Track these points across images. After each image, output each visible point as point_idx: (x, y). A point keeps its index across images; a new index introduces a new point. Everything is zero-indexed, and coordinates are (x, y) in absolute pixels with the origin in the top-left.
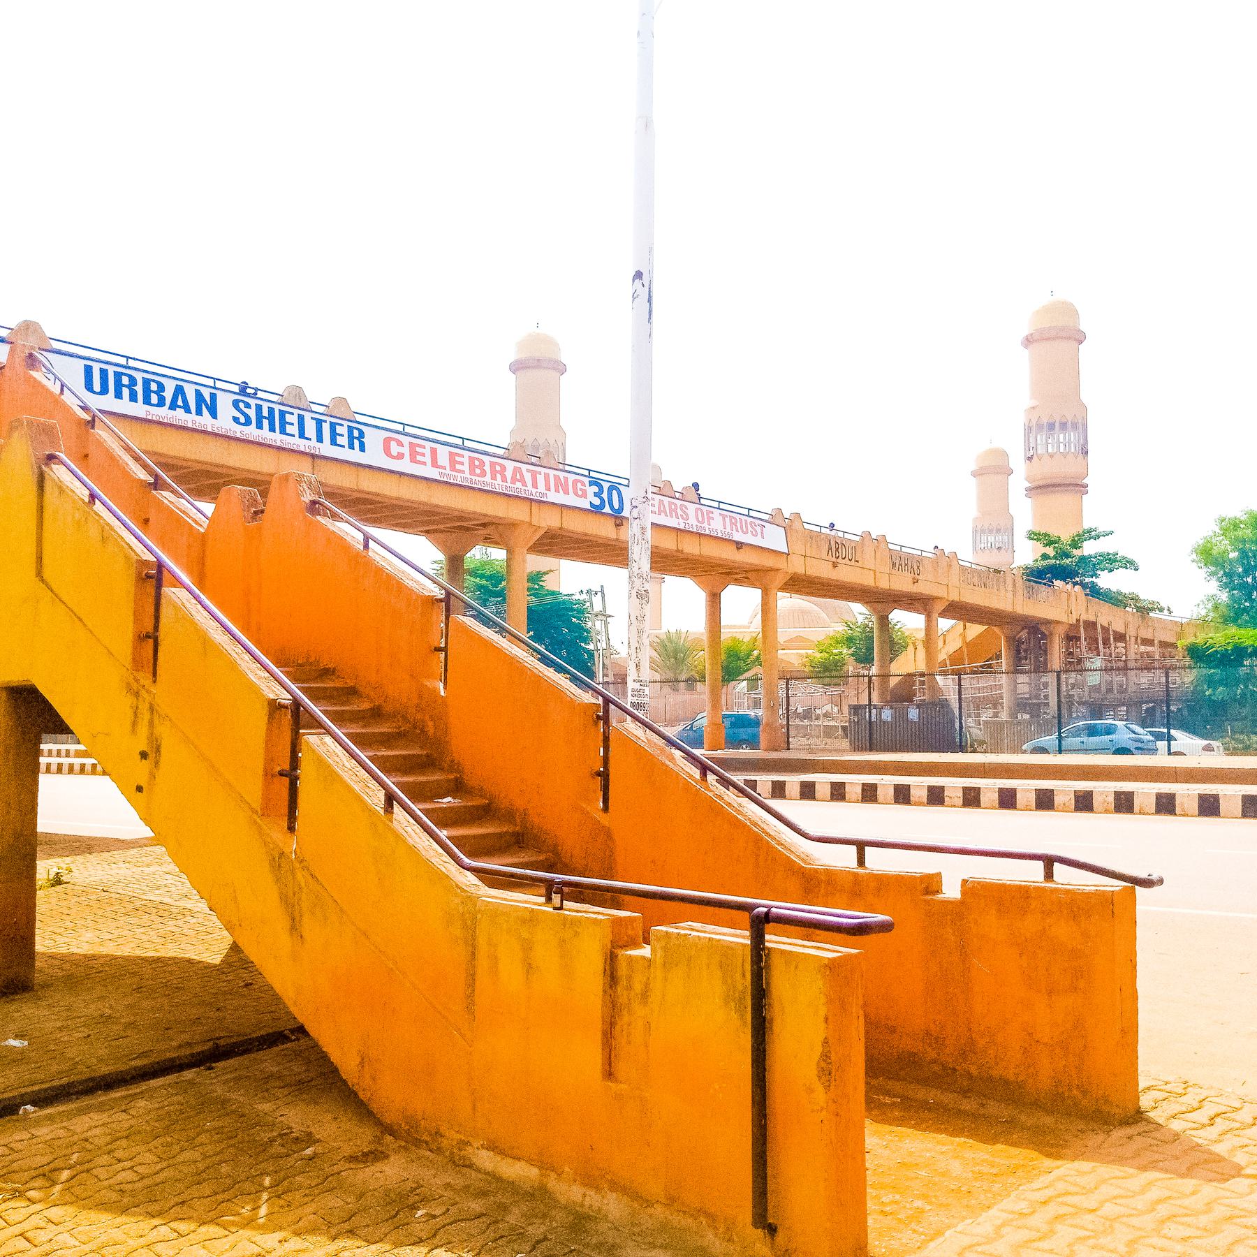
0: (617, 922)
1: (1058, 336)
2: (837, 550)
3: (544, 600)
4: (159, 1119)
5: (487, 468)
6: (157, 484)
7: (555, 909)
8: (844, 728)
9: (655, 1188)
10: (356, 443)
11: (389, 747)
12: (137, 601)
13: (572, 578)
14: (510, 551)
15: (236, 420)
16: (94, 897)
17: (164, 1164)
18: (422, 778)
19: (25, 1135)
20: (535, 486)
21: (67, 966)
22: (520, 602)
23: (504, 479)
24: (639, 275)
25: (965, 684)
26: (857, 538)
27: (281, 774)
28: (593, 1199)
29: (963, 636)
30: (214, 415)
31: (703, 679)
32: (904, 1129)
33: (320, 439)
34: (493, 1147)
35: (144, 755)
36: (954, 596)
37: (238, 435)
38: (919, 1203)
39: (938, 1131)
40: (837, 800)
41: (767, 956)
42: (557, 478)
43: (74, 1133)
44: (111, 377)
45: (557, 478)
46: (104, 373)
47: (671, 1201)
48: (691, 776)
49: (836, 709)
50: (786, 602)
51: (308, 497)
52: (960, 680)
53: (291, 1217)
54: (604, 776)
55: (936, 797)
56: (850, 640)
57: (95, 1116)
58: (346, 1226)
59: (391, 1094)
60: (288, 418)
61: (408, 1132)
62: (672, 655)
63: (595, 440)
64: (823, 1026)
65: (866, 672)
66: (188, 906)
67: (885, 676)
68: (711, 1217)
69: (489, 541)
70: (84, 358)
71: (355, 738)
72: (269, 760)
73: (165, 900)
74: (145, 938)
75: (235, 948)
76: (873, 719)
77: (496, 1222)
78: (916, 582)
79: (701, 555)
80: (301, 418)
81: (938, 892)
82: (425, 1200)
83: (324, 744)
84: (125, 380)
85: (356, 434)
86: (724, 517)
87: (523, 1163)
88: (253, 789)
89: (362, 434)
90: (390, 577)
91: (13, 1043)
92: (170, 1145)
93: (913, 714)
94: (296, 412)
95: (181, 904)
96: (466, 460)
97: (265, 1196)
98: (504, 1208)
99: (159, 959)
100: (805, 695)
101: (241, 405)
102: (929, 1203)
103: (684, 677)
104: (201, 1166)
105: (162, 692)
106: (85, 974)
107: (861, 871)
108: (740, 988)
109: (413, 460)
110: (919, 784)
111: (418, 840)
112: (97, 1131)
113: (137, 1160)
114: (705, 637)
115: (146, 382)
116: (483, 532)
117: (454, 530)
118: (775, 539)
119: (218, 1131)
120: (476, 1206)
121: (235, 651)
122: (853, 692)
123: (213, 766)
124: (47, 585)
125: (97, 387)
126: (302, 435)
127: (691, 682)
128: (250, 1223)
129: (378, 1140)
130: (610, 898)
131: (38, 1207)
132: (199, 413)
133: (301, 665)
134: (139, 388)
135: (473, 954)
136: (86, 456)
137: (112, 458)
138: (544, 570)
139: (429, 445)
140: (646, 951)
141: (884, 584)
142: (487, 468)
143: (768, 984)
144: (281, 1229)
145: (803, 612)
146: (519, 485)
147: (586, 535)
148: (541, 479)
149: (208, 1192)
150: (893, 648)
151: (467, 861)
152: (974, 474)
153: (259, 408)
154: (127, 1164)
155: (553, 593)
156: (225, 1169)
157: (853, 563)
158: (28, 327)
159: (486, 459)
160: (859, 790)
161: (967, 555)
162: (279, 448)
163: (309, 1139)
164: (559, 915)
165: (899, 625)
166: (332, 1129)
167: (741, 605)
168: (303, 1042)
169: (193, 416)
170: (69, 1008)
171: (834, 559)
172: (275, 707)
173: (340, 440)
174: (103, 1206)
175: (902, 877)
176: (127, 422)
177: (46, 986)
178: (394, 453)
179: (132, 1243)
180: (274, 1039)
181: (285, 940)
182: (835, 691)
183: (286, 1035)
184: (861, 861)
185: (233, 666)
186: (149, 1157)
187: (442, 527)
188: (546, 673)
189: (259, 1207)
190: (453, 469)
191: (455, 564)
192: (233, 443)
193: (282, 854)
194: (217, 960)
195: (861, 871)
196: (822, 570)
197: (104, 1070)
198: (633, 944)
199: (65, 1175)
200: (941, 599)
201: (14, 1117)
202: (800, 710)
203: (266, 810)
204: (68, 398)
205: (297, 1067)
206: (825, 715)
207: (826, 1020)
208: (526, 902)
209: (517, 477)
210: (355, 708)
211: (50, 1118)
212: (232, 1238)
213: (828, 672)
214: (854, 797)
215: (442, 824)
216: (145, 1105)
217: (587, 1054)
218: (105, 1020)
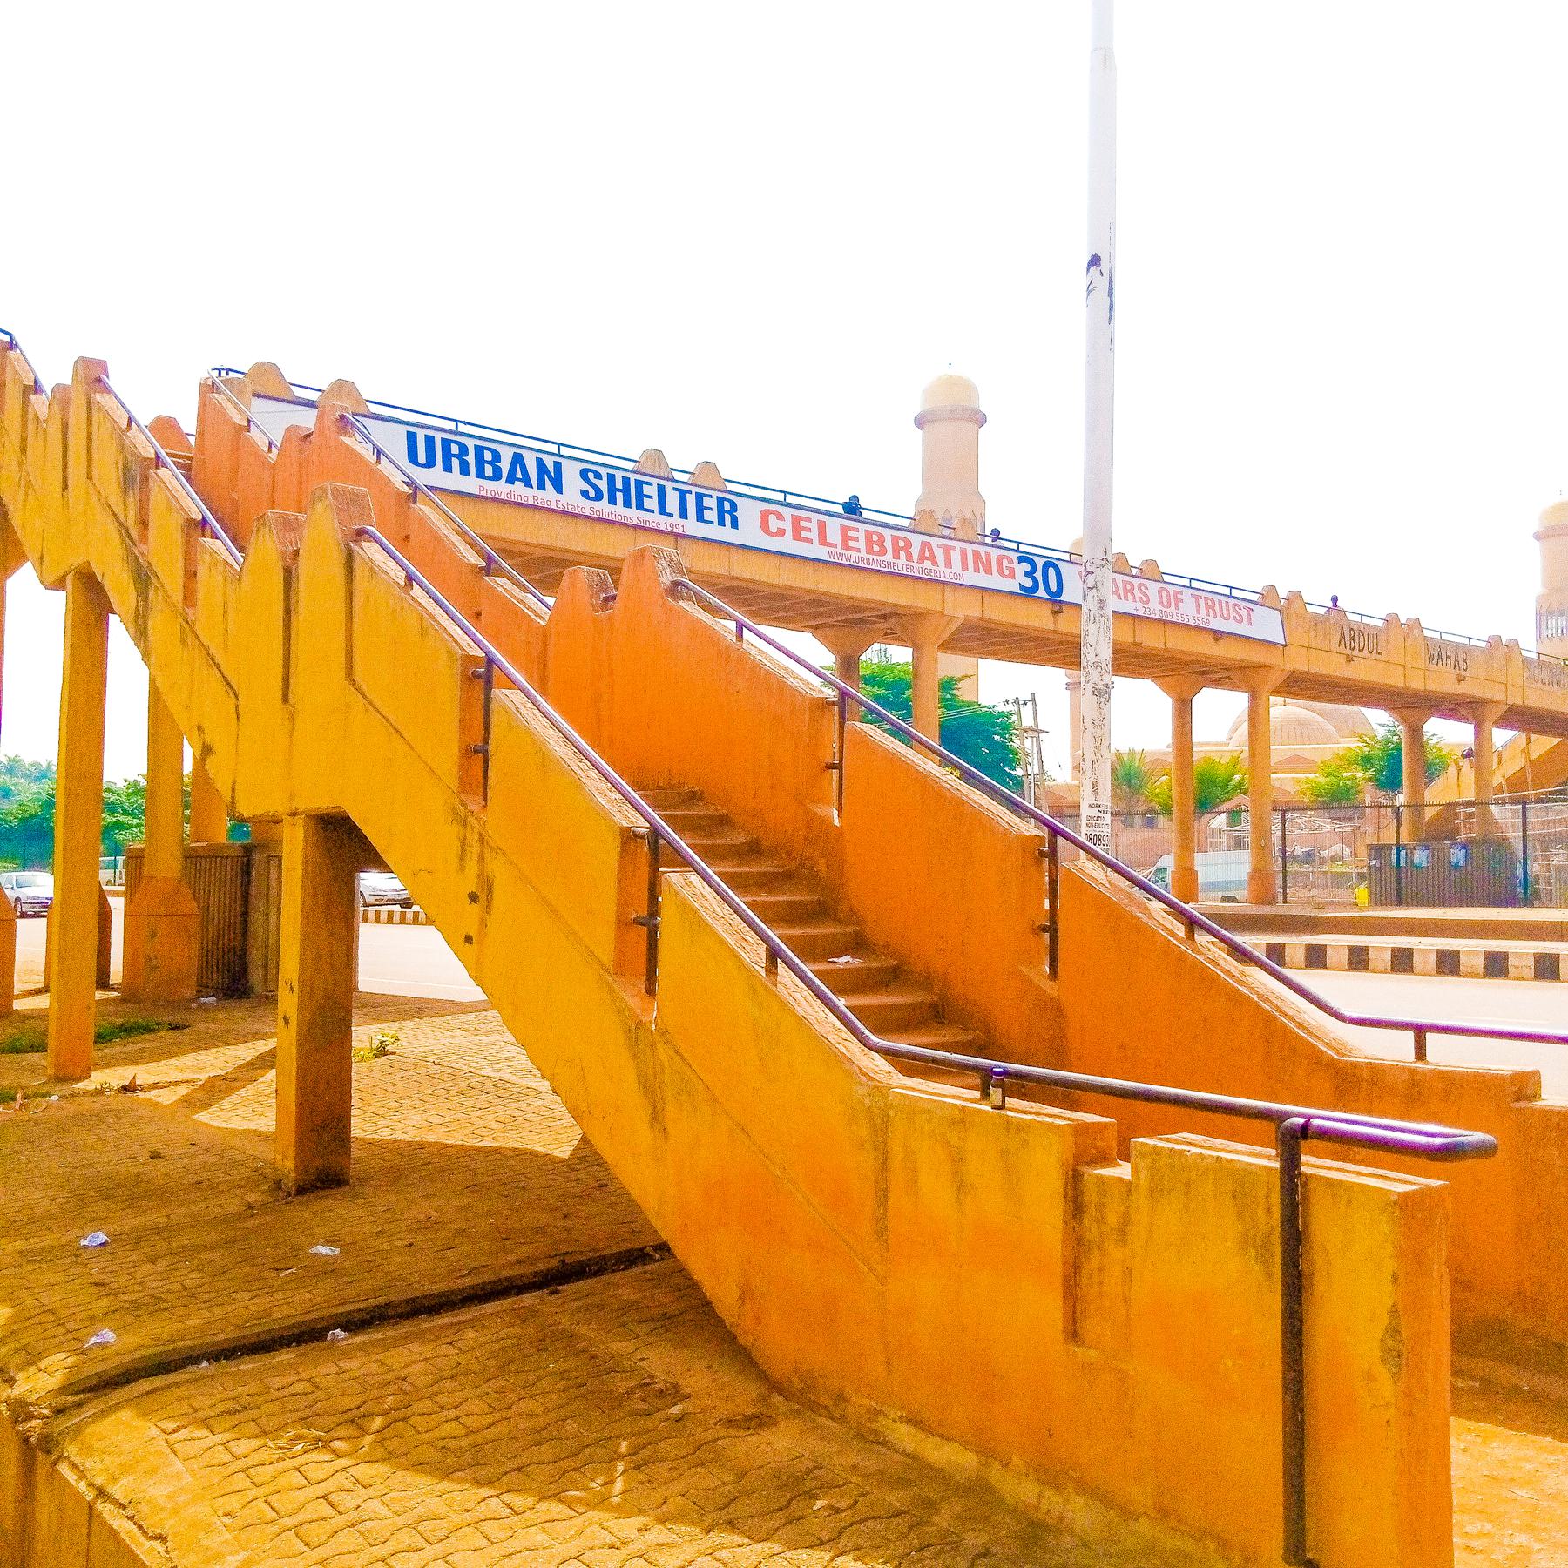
0: (1081, 1130)
2: (1352, 639)
3: (958, 713)
4: (491, 1355)
5: (888, 544)
6: (490, 568)
7: (995, 1108)
8: (1361, 877)
9: (1140, 1495)
10: (728, 518)
11: (770, 892)
12: (465, 706)
13: (996, 683)
14: (917, 649)
15: (585, 494)
16: (423, 1071)
17: (497, 1416)
18: (810, 931)
19: (333, 1369)
20: (948, 564)
21: (388, 1156)
22: (930, 717)
23: (909, 557)
24: (1095, 261)
25: (1531, 817)
26: (1380, 623)
27: (638, 922)
28: (1052, 1503)
29: (1526, 751)
30: (559, 490)
31: (1167, 812)
32: (1489, 1426)
33: (684, 515)
34: (914, 1421)
35: (473, 898)
36: (1515, 699)
37: (587, 513)
38: (1522, 1539)
39: (1537, 1432)
40: (1357, 969)
41: (1305, 1185)
42: (976, 554)
43: (390, 1369)
44: (440, 446)
45: (976, 554)
46: (430, 441)
47: (1163, 1513)
48: (1172, 934)
49: (1347, 851)
50: (1281, 709)
51: (667, 578)
52: (1524, 809)
53: (657, 1497)
54: (1052, 929)
55: (1496, 966)
56: (1366, 761)
57: (415, 1347)
58: (721, 1515)
59: (781, 1343)
60: (647, 490)
61: (801, 1391)
62: (1128, 779)
63: (1031, 503)
64: (1390, 1288)
65: (1389, 803)
66: (533, 1085)
67: (1417, 807)
68: (1223, 1544)
69: (890, 636)
70: (407, 424)
71: (729, 879)
72: (623, 903)
73: (508, 1077)
74: (481, 1123)
75: (584, 1140)
76: (1402, 864)
77: (920, 1524)
79: (1166, 649)
80: (661, 489)
81: (1536, 1096)
82: (827, 1486)
83: (689, 884)
84: (455, 449)
85: (727, 506)
86: (1197, 598)
87: (956, 1445)
88: (604, 942)
89: (734, 506)
90: (768, 675)
91: (322, 1250)
92: (502, 1391)
93: (1457, 856)
94: (655, 481)
95: (525, 1081)
96: (861, 536)
97: (621, 1467)
98: (930, 1505)
99: (496, 1151)
100: (1308, 831)
101: (591, 475)
102: (1541, 1541)
103: (1141, 808)
104: (543, 1421)
105: (495, 820)
106: (413, 1166)
107: (1420, 1065)
108: (1262, 1227)
109: (797, 537)
110: (1473, 949)
111: (810, 1010)
112: (416, 1368)
113: (464, 1408)
114: (1171, 759)
115: (479, 451)
116: (884, 626)
117: (848, 624)
118: (1267, 626)
119: (563, 1374)
120: (895, 1499)
121: (580, 767)
122: (1371, 829)
123: (555, 912)
124: (359, 690)
125: (422, 458)
126: (662, 510)
127: (1149, 818)
128: (602, 1502)
129: (763, 1399)
130: (1065, 1094)
131: (345, 1462)
132: (541, 486)
133: (660, 788)
134: (471, 458)
135: (885, 1162)
136: (408, 537)
137: (437, 539)
138: (957, 675)
139: (815, 517)
140: (1124, 1171)
141: (1417, 684)
142: (888, 544)
143: (1305, 1225)
144: (640, 1512)
145: (1301, 724)
146: (928, 564)
147: (1015, 626)
148: (956, 556)
149: (546, 1457)
150: (1428, 771)
151: (873, 1038)
152: (1537, 537)
153: (611, 478)
154: (453, 1413)
155: (970, 704)
156: (571, 1426)
157: (1374, 655)
158: (343, 387)
159: (887, 533)
160: (1388, 956)
161: (1529, 645)
162: (635, 527)
163: (675, 1393)
164: (1001, 1116)
165: (1435, 740)
166: (704, 1381)
167: (1220, 714)
168: (669, 1262)
169: (535, 491)
170: (389, 1209)
171: (1348, 651)
172: (628, 837)
173: (708, 515)
174: (419, 1466)
175: (1483, 1076)
176: (452, 497)
177: (363, 1180)
178: (773, 529)
179: (456, 1519)
180: (633, 1258)
181: (644, 1135)
182: (1348, 827)
183: (644, 1254)
184: (1420, 1051)
185: (578, 784)
186: (477, 1406)
187: (830, 620)
188: (971, 795)
189: (612, 1482)
190: (846, 546)
191: (848, 665)
192: (581, 523)
193: (639, 1024)
194: (565, 1153)
195: (1420, 1065)
196: (1331, 666)
197: (429, 1288)
198: (1104, 1159)
199: (378, 1422)
200: (1498, 702)
201: (322, 1344)
202: (1299, 852)
203: (620, 969)
204: (385, 466)
205: (662, 1296)
206: (1334, 859)
207: (1395, 1278)
208: (954, 1097)
209: (927, 554)
210: (728, 841)
211: (362, 1347)
212: (579, 1520)
213: (1337, 802)
214: (1381, 966)
215: (839, 992)
216: (482, 1333)
217: (1052, 1308)
218: (431, 1224)
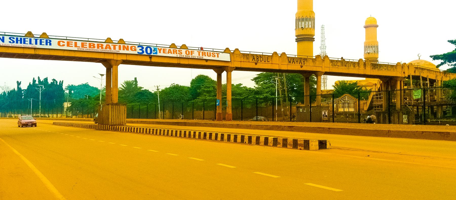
1: (371, 26)
15: (10, 42)
78: (302, 67)
89: (50, 41)
126: (30, 43)
146: (108, 49)
162: (24, 48)
171: (256, 61)
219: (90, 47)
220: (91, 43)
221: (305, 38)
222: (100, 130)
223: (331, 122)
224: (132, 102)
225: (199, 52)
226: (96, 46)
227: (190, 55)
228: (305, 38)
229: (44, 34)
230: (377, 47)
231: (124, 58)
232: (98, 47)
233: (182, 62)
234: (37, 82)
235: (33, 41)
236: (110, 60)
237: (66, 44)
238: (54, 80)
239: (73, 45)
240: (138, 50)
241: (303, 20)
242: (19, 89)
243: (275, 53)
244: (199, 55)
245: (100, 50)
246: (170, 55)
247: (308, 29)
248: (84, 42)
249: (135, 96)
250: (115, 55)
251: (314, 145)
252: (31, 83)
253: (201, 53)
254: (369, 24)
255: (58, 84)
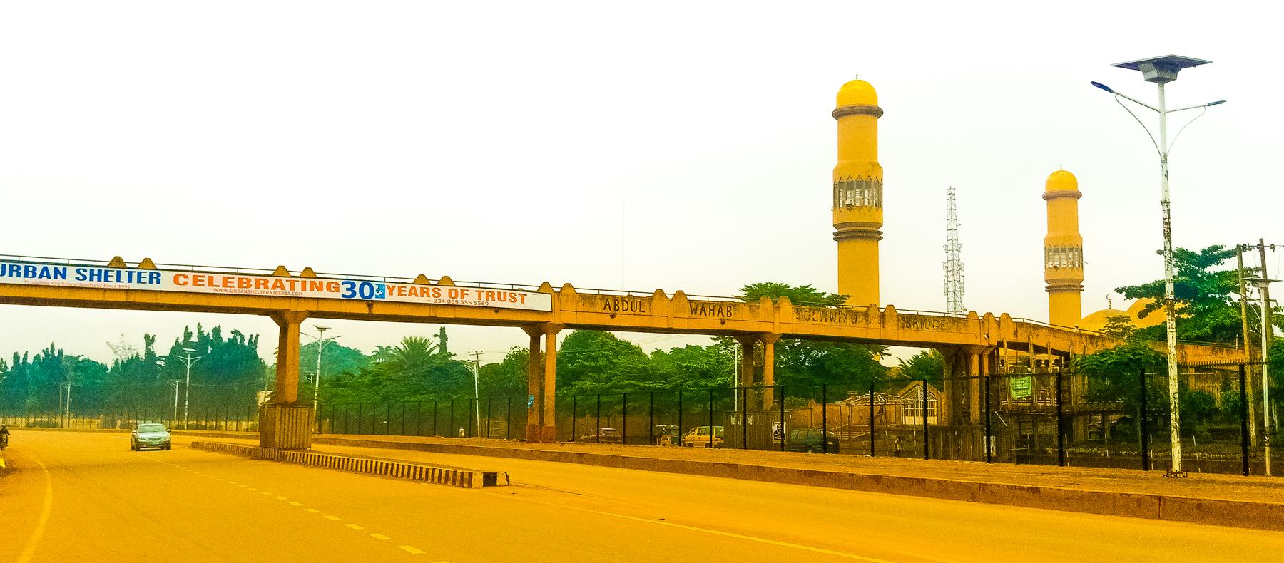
1: (858, 112)
78: (723, 323)
89: (159, 275)
126: (118, 280)
134: (22, 271)
146: (278, 290)
219: (240, 286)
220: (244, 277)
221: (858, 233)
222: (262, 459)
223: (860, 451)
224: (417, 392)
225: (480, 293)
226: (253, 283)
227: (459, 299)
228: (858, 233)
229: (147, 260)
230: (1080, 250)
231: (313, 307)
232: (257, 286)
233: (441, 313)
234: (194, 339)
235: (124, 276)
236: (283, 311)
237: (190, 280)
238: (236, 332)
239: (206, 283)
240: (344, 290)
241: (850, 185)
242: (150, 354)
243: (660, 293)
244: (480, 298)
245: (261, 291)
246: (413, 299)
247: (864, 210)
248: (227, 276)
249: (425, 377)
250: (294, 302)
251: (478, 479)
252: (181, 341)
253: (484, 295)
254: (1056, 189)
255: (246, 343)
